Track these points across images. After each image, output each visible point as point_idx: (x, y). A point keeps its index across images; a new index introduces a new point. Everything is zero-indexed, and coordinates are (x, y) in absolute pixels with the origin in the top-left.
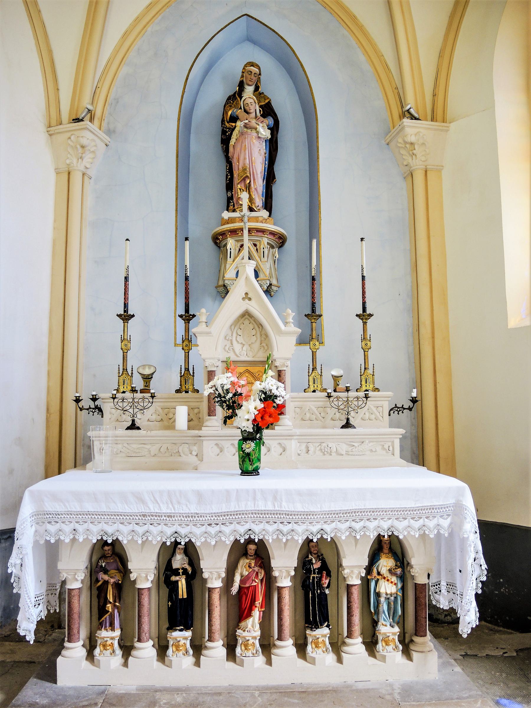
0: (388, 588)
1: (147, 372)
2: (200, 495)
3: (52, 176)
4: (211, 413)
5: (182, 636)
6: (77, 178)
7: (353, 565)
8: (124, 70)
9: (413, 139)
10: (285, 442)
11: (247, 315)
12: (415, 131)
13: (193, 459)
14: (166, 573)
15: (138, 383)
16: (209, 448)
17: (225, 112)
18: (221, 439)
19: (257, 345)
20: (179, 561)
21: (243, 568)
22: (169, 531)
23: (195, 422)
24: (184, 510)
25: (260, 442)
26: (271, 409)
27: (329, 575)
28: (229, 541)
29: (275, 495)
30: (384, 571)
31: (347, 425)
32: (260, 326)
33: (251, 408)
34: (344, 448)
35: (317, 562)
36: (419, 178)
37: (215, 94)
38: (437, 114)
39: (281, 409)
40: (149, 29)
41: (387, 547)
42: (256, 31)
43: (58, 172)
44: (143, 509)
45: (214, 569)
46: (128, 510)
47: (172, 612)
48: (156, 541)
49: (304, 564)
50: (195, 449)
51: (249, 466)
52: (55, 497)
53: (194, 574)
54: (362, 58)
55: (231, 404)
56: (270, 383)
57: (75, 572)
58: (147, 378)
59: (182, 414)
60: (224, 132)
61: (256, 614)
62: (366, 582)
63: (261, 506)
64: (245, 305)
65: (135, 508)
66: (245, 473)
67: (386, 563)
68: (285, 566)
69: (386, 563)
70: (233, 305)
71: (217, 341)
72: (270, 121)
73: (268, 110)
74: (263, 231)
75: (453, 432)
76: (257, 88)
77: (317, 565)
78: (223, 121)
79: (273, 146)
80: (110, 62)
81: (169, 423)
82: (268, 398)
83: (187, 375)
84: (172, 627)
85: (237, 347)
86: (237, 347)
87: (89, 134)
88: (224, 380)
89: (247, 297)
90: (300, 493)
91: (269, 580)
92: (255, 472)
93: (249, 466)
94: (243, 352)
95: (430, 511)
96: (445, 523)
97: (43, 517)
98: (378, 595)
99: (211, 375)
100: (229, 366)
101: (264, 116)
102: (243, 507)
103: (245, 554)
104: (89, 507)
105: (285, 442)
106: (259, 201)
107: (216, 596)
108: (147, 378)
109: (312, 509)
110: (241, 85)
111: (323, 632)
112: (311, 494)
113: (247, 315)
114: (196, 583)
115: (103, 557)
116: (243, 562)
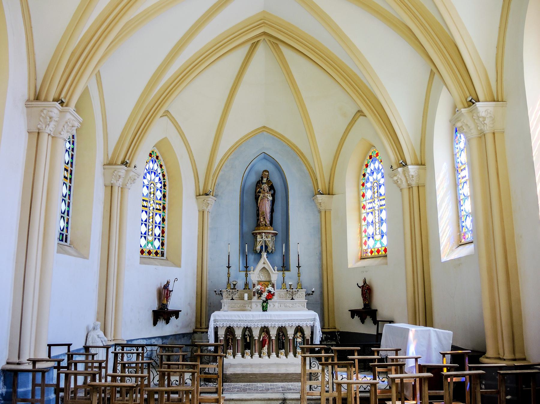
0: (299, 340)
1: (235, 283)
2: (253, 316)
3: (197, 213)
4: (254, 295)
5: (248, 351)
6: (206, 213)
7: (290, 333)
8: (221, 173)
9: (320, 201)
10: (275, 304)
11: (264, 268)
12: (321, 198)
13: (249, 308)
14: (244, 335)
15: (232, 287)
16: (254, 305)
17: (256, 189)
18: (257, 302)
19: (267, 276)
20: (247, 333)
21: (263, 335)
22: (246, 324)
23: (250, 298)
24: (249, 319)
25: (267, 303)
26: (271, 295)
27: (284, 337)
28: (260, 326)
29: (271, 316)
30: (298, 336)
31: (292, 299)
32: (268, 271)
33: (265, 294)
34: (291, 305)
35: (282, 331)
36: (323, 213)
37: (253, 179)
38: (330, 193)
39: (273, 295)
40: (229, 157)
41: (299, 329)
42: (267, 157)
43: (199, 211)
44: (239, 319)
45: (256, 334)
46: (236, 319)
47: (245, 345)
48: (243, 326)
49: (278, 335)
50: (250, 305)
51: (264, 309)
52: (219, 316)
53: (251, 336)
54: (305, 168)
55: (260, 294)
56: (270, 288)
57: (222, 334)
58: (235, 285)
59: (246, 296)
60: (256, 195)
61: (266, 346)
62: (294, 338)
63: (268, 318)
64: (264, 266)
65: (238, 319)
66: (264, 311)
67: (299, 334)
68: (273, 333)
69: (299, 334)
70: (260, 265)
71: (255, 276)
72: (272, 192)
73: (272, 188)
74: (269, 233)
75: (334, 303)
76: (267, 179)
77: (281, 334)
78: (256, 192)
79: (273, 202)
80: (216, 170)
81: (242, 298)
82: (269, 292)
83: (246, 284)
84: (245, 349)
85: (261, 277)
86: (261, 277)
87: (211, 199)
88: (258, 287)
89: (264, 263)
90: (277, 315)
91: (270, 337)
92: (266, 310)
93: (264, 309)
94: (263, 278)
95: (308, 320)
96: (312, 323)
97: (215, 321)
98: (297, 342)
99: (254, 285)
100: (259, 282)
101: (270, 190)
102: (263, 318)
103: (264, 331)
104: (227, 318)
105: (275, 304)
106: (268, 223)
107: (256, 341)
108: (235, 285)
109: (281, 319)
110: (262, 178)
111: (283, 351)
112: (279, 315)
113: (264, 268)
114: (251, 339)
115: (228, 332)
116: (263, 333)
